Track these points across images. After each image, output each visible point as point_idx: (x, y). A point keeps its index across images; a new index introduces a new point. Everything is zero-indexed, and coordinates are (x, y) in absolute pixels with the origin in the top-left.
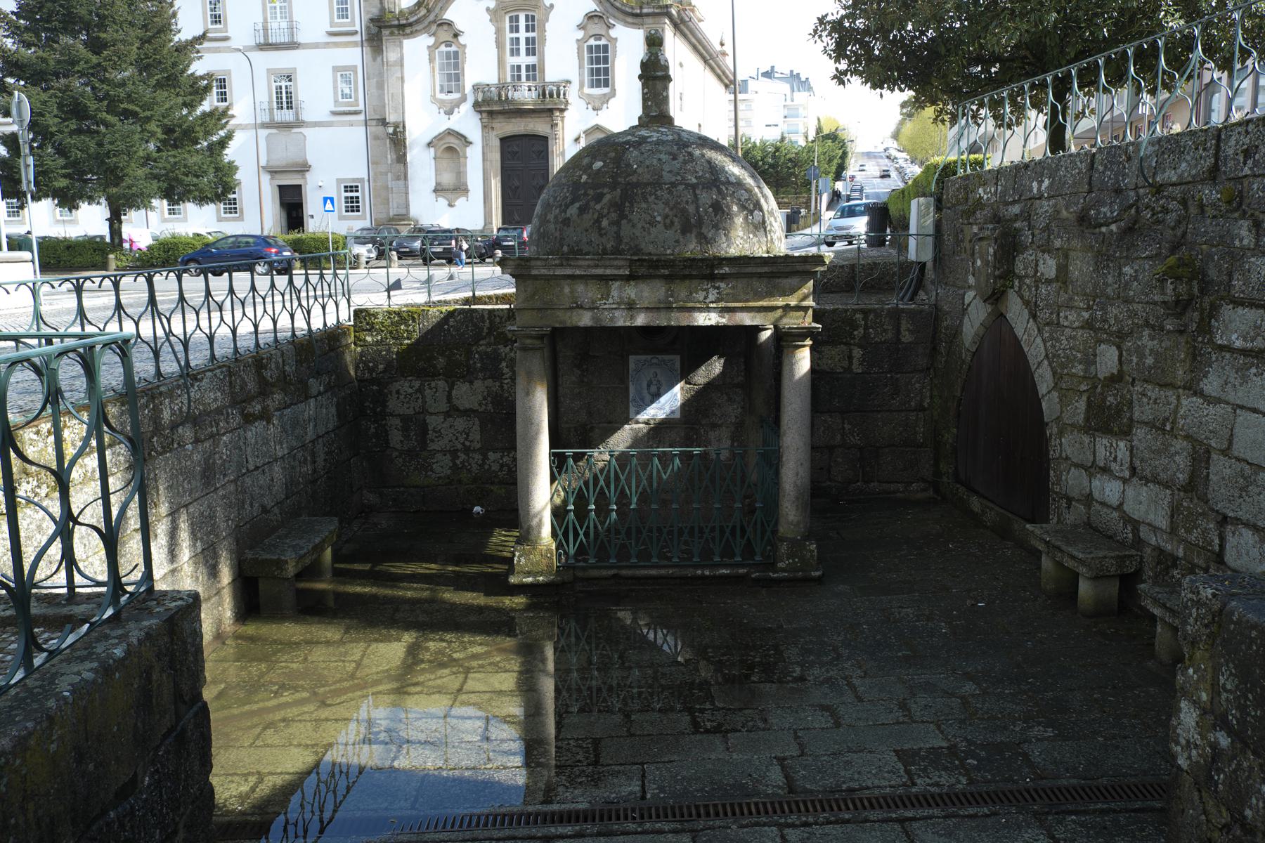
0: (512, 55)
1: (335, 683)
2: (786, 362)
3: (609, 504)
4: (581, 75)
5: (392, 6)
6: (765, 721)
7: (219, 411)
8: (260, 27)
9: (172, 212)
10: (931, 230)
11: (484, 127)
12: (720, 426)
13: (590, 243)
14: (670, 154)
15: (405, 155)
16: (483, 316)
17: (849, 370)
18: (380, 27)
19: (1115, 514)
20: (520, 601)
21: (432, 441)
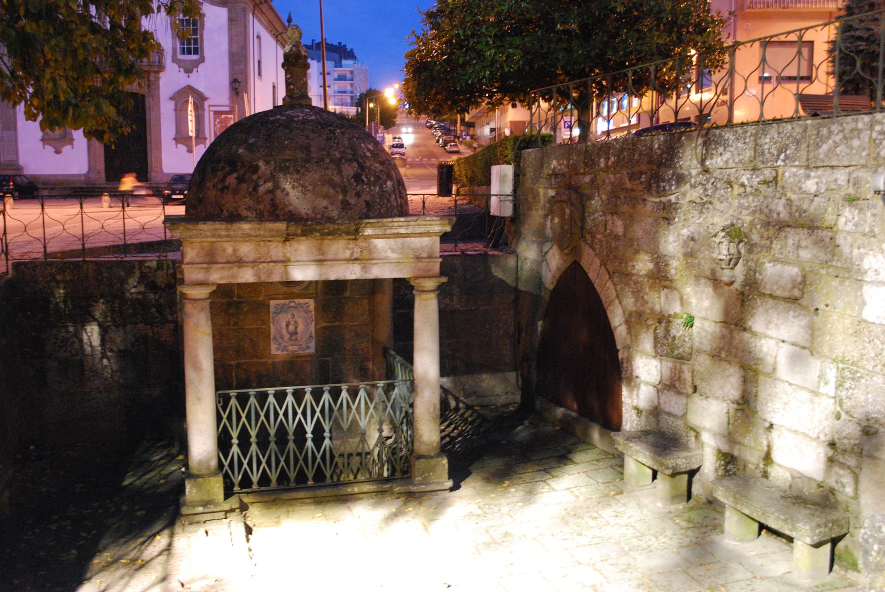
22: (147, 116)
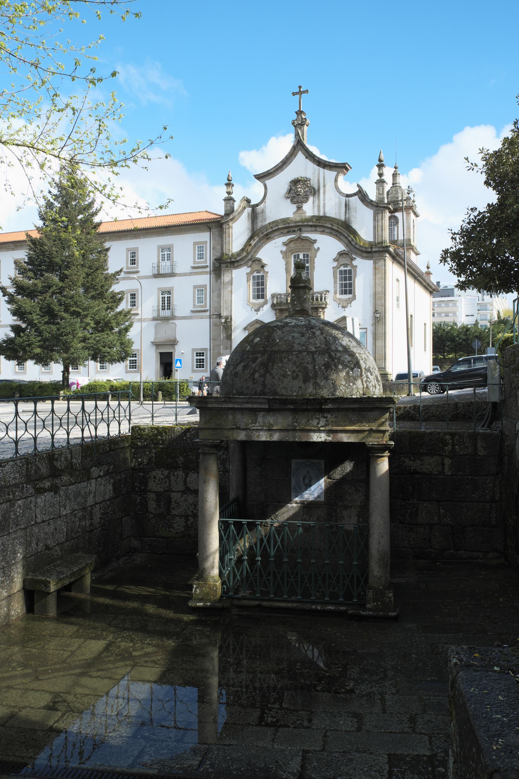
1: (51, 665)
2: (371, 466)
4: (335, 287)
5: (227, 252)
6: (310, 720)
7: (16, 485)
8: (156, 265)
9: (102, 368)
13: (248, 388)
14: (300, 333)
15: (231, 335)
18: (220, 263)
21: (174, 509)
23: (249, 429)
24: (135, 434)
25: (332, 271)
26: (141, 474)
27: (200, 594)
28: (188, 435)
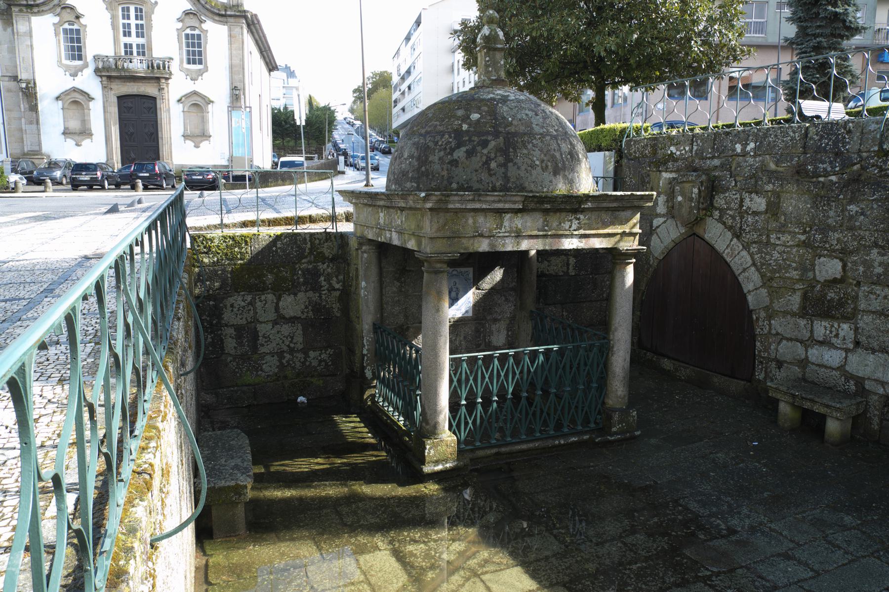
0: (125, 35)
3: (476, 398)
4: (181, 54)
10: (612, 174)
11: (104, 88)
12: (499, 320)
13: (480, 181)
15: (36, 105)
16: (305, 239)
17: (566, 273)
18: (10, 5)
19: (837, 373)
20: (431, 488)
21: (262, 345)
22: (159, 117)
23: (493, 236)
24: (199, 246)
25: (176, 33)
26: (211, 303)
27: (435, 455)
28: (279, 244)
